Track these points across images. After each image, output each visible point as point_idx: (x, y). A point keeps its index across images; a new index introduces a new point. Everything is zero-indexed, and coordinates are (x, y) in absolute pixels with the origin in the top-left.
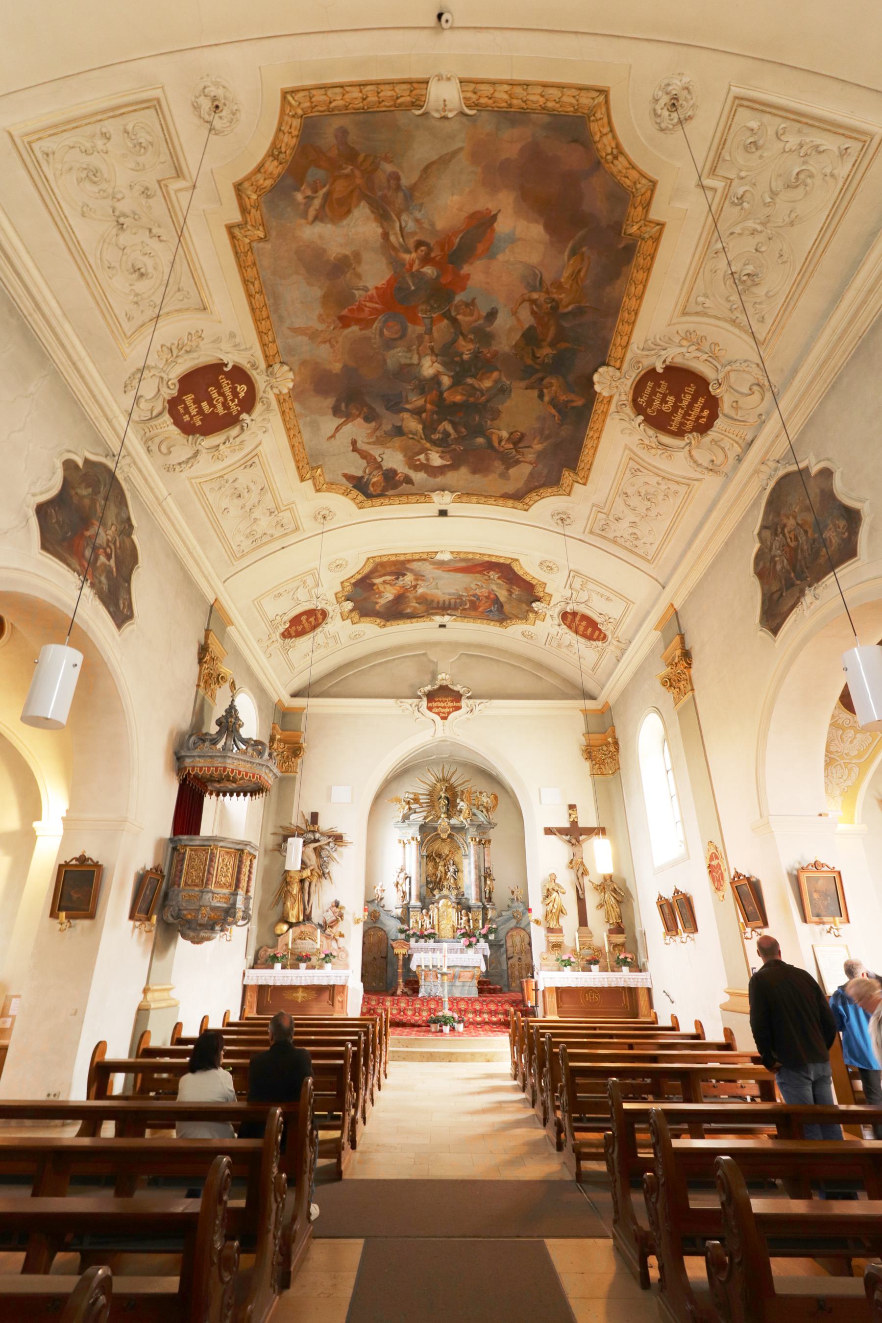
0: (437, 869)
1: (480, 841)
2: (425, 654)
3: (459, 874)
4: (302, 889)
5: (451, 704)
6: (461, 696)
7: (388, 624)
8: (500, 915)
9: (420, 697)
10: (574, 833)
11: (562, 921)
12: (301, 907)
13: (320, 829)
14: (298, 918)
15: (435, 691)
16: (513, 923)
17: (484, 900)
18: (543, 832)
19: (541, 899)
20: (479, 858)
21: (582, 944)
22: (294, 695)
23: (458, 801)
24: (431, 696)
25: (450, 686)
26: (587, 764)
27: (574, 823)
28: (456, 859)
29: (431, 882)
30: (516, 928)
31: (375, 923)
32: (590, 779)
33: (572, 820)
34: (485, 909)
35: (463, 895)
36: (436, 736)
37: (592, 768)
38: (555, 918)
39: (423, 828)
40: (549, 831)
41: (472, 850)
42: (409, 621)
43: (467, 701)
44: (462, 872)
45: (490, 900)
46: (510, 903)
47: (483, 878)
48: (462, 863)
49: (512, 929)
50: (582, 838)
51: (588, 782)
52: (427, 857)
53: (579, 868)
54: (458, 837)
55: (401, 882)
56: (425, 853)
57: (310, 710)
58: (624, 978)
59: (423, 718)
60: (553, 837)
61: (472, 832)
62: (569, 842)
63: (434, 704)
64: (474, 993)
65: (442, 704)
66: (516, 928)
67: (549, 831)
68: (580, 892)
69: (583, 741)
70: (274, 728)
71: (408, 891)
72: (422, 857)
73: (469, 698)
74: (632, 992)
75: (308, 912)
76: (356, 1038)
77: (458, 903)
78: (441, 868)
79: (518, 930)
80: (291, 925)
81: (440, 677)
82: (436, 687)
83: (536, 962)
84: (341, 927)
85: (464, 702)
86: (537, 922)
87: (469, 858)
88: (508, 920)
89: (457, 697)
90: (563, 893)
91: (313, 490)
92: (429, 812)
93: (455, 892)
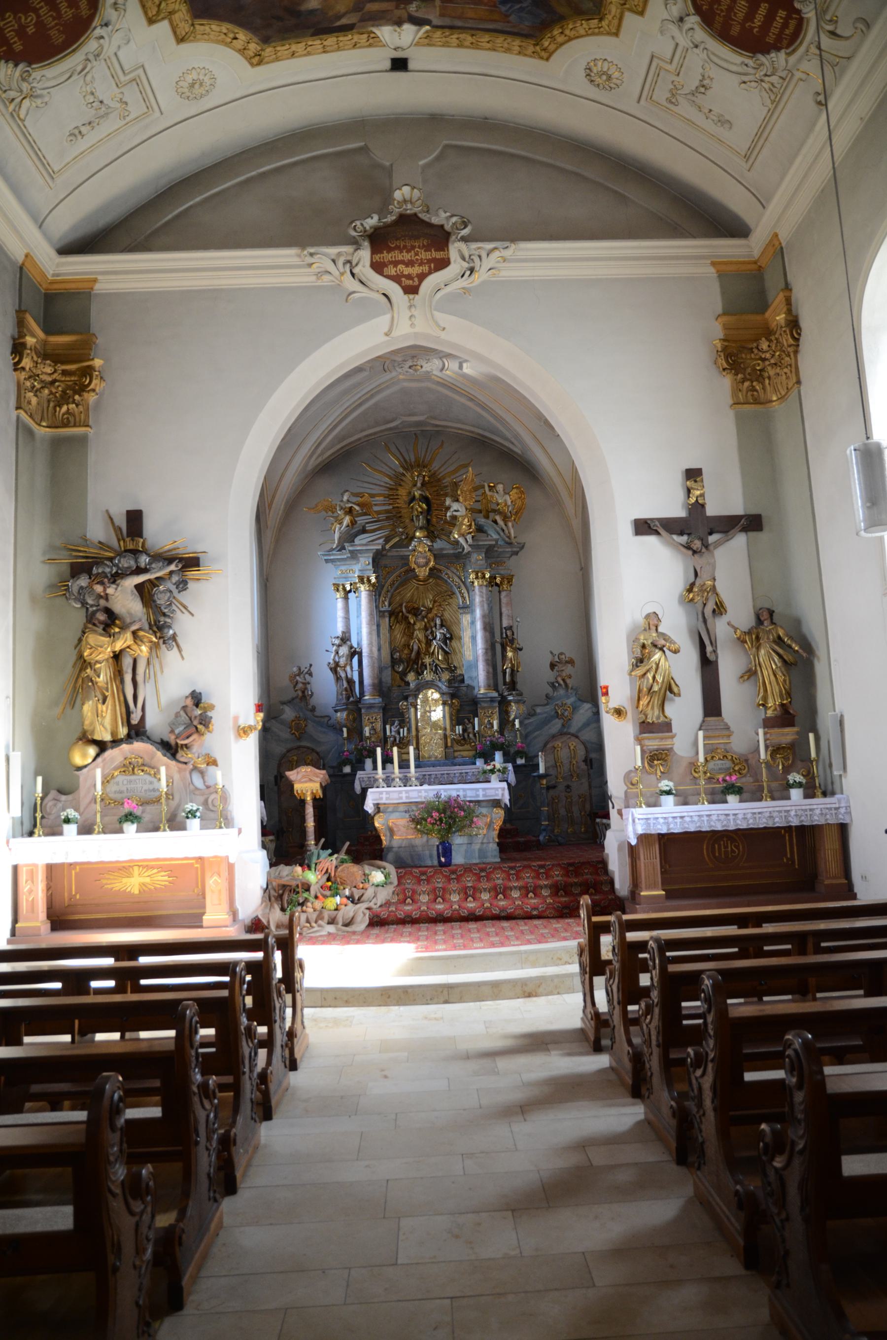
0: (411, 636)
1: (492, 578)
2: (364, 150)
3: (454, 643)
4: (119, 674)
5: (424, 255)
6: (448, 235)
7: (269, 51)
8: (531, 714)
9: (355, 243)
10: (694, 529)
11: (671, 710)
12: (120, 710)
13: (149, 544)
14: (114, 733)
15: (387, 226)
16: (556, 726)
17: (502, 687)
18: (629, 529)
19: (627, 667)
20: (491, 609)
21: (711, 752)
22: (66, 250)
23: (448, 501)
24: (378, 240)
25: (422, 216)
26: (726, 382)
27: (697, 508)
28: (447, 615)
29: (400, 661)
30: (561, 734)
31: (299, 739)
32: (731, 414)
33: (693, 500)
34: (503, 703)
35: (463, 681)
36: (396, 333)
37: (736, 391)
38: (656, 701)
39: (377, 560)
40: (643, 527)
41: (478, 598)
42: (317, 42)
43: (462, 246)
44: (460, 638)
45: (512, 686)
46: (549, 690)
47: (498, 648)
48: (458, 622)
49: (554, 737)
50: (712, 539)
51: (728, 420)
52: (392, 614)
53: (702, 598)
54: (451, 576)
55: (342, 661)
56: (386, 607)
57: (103, 286)
58: (796, 808)
59: (363, 292)
60: (652, 539)
61: (478, 558)
62: (688, 547)
63: (387, 256)
64: (492, 852)
65: (407, 256)
66: (561, 734)
67: (643, 527)
68: (709, 649)
69: (717, 331)
70: (21, 323)
71: (356, 678)
72: (381, 614)
73: (464, 239)
74: (806, 835)
75: (135, 719)
76: (259, 955)
77: (453, 696)
78: (419, 634)
79: (565, 738)
80: (102, 747)
81: (398, 195)
82: (390, 219)
83: (615, 785)
84: (201, 745)
85: (455, 249)
86: (619, 712)
87: (472, 612)
88: (547, 721)
89: (440, 238)
90: (676, 652)
91: (172, 40)
92: (394, 527)
93: (446, 676)
